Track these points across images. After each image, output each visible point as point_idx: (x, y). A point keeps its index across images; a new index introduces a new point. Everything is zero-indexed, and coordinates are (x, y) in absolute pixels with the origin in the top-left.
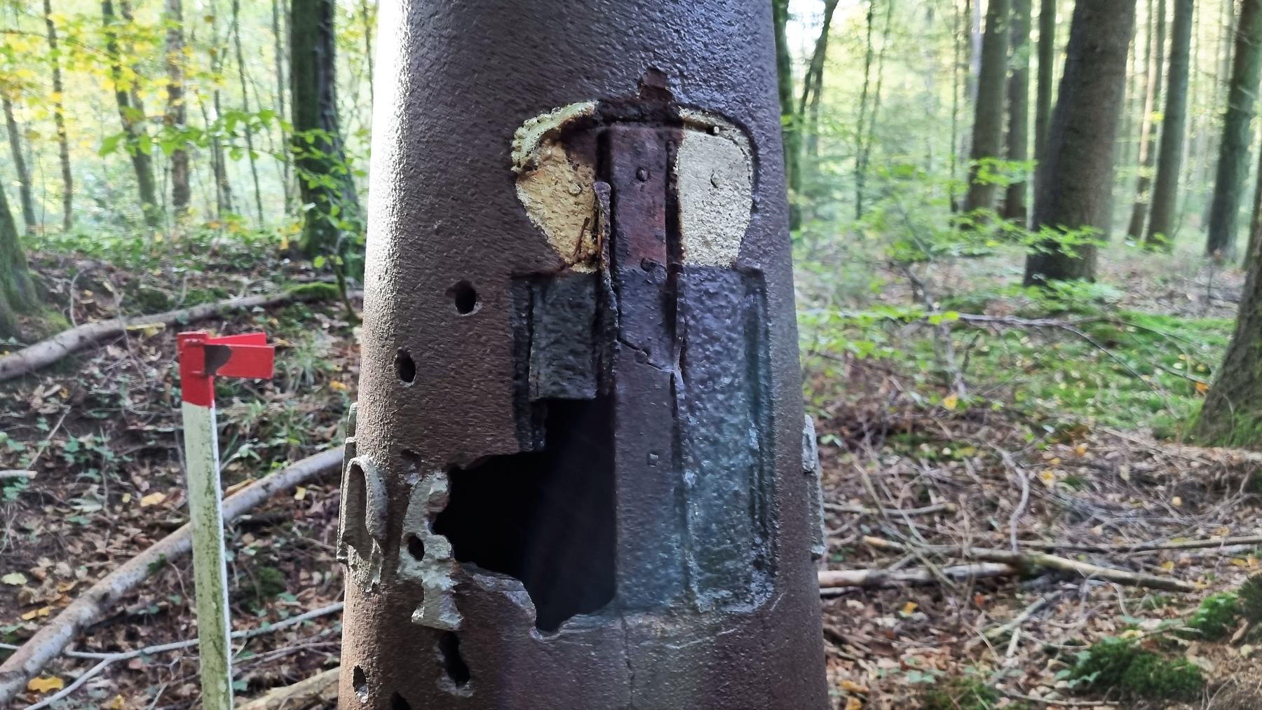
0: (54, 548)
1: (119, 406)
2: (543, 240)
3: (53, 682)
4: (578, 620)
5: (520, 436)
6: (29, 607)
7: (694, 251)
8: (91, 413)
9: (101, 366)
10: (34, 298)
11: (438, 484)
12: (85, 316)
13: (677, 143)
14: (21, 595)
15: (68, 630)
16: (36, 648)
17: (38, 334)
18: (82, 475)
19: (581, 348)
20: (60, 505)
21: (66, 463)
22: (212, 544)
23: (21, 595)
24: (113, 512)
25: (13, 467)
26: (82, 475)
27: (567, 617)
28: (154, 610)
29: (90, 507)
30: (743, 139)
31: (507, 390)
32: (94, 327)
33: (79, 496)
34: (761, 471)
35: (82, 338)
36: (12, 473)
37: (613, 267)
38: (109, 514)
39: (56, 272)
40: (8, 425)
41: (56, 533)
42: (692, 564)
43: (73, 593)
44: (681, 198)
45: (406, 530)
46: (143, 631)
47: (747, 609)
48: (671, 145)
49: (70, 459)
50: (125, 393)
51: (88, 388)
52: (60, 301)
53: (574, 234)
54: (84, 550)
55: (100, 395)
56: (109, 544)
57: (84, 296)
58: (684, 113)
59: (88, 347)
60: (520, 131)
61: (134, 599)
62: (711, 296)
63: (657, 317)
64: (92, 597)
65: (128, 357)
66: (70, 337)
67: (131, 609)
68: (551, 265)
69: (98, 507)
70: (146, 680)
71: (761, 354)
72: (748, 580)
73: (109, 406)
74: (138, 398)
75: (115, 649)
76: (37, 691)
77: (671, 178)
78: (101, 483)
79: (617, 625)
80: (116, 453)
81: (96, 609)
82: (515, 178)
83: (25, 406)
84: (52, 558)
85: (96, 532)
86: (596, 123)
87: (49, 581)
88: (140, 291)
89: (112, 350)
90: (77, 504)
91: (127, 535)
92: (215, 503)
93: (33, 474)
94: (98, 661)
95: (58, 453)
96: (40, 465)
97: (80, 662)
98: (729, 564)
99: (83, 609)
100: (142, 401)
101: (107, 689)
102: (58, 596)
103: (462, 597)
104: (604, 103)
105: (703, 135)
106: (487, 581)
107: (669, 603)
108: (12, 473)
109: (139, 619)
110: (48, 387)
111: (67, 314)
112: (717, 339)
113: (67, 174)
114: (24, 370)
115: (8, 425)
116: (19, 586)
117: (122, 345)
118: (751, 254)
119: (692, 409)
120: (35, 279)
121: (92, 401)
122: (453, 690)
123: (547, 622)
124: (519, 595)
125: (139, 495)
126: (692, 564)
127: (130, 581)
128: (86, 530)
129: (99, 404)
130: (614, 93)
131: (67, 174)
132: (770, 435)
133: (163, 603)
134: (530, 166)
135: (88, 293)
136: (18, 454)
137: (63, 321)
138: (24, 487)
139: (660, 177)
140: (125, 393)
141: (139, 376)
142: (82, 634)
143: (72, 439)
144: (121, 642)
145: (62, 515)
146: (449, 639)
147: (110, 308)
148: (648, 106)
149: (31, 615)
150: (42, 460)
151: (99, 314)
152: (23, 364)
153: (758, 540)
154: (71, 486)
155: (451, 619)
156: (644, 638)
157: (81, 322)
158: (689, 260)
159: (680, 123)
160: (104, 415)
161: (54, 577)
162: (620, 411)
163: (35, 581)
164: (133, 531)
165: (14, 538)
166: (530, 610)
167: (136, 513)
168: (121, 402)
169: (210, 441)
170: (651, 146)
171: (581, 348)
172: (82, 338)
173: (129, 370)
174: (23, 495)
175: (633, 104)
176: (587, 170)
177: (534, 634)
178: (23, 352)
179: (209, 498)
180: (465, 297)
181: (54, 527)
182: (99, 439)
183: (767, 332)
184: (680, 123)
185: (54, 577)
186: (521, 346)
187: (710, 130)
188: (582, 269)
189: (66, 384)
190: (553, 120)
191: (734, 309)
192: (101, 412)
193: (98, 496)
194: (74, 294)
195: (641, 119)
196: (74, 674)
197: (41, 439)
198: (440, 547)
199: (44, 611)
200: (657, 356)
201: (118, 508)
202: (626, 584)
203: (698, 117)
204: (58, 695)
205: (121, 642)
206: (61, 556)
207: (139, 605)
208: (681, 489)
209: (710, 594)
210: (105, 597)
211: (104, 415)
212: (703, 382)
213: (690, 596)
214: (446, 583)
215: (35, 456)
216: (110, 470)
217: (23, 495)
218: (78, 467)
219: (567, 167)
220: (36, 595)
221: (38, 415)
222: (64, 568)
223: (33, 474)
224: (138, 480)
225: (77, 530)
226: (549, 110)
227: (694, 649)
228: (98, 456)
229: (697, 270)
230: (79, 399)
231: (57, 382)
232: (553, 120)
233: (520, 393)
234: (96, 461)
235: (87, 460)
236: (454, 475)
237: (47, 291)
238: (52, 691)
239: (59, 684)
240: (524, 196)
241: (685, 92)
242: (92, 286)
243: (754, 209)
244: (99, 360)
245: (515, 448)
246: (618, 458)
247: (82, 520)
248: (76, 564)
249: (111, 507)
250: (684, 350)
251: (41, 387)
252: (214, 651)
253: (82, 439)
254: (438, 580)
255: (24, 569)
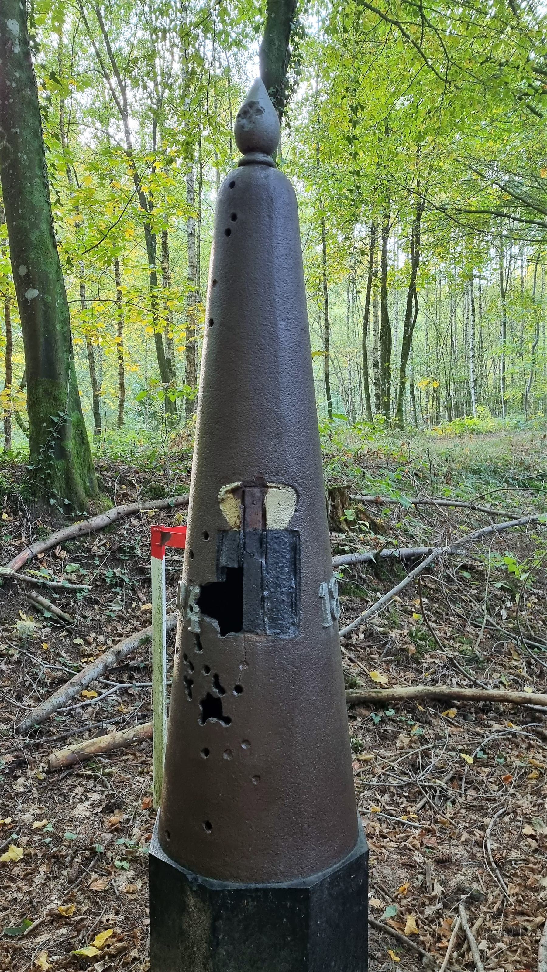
0: (98, 628)
1: (134, 553)
2: (226, 520)
3: (93, 693)
4: (232, 633)
5: (218, 577)
6: (84, 656)
7: (271, 524)
8: (120, 556)
9: (127, 529)
10: (97, 490)
11: (197, 590)
12: (121, 500)
13: (266, 493)
14: (81, 650)
15: (101, 667)
16: (86, 674)
17: (98, 510)
18: (113, 590)
19: (233, 552)
20: (102, 605)
21: (106, 583)
22: (160, 622)
23: (81, 650)
24: (127, 612)
25: (81, 583)
26: (113, 590)
27: (229, 632)
28: (142, 665)
29: (116, 608)
30: (292, 490)
31: (214, 563)
32: (126, 507)
33: (111, 601)
34: (296, 595)
35: (119, 513)
36: (81, 586)
37: (244, 529)
38: (125, 613)
39: (109, 474)
40: (80, 560)
41: (99, 620)
42: (266, 620)
43: (104, 651)
44: (267, 509)
45: (189, 603)
46: (136, 676)
47: (287, 637)
48: (264, 493)
49: (108, 581)
50: (138, 546)
51: (120, 542)
52: (108, 490)
53: (234, 519)
54: (112, 630)
55: (125, 546)
56: (123, 629)
57: (121, 488)
58: (269, 484)
59: (120, 519)
60: (221, 489)
61: (133, 659)
62: (276, 538)
63: (257, 544)
64: (113, 651)
65: (141, 525)
66: (113, 513)
67: (131, 663)
68: (228, 528)
69: (120, 608)
70: (135, 699)
71: (298, 557)
72: (288, 628)
73: (129, 553)
74: (144, 549)
75: (122, 682)
76: (86, 697)
77: (263, 504)
78: (122, 595)
79: (242, 636)
80: (131, 579)
81: (114, 658)
82: (219, 502)
83: (89, 550)
84: (96, 633)
85: (118, 622)
86: (241, 488)
87: (94, 645)
88: (152, 487)
89: (134, 521)
90: (110, 606)
91: (133, 625)
92: (162, 603)
93: (90, 587)
94: (113, 686)
95: (103, 577)
96: (94, 583)
97: (106, 686)
98: (280, 622)
99: (109, 658)
100: (146, 551)
101: (117, 701)
102: (98, 652)
103: (201, 624)
104: (244, 482)
105: (275, 490)
106: (207, 619)
107: (259, 631)
108: (81, 586)
109: (134, 669)
110: (100, 540)
111: (113, 499)
112: (278, 552)
113: (122, 384)
114: (90, 530)
115: (80, 560)
116: (80, 645)
117: (139, 518)
118: (293, 525)
119: (268, 572)
120: (98, 479)
121: (121, 550)
122: (198, 652)
123: (223, 633)
124: (215, 624)
125: (141, 604)
126: (266, 620)
127: (131, 646)
128: (113, 620)
129: (125, 552)
130: (247, 479)
131: (122, 384)
132: (300, 583)
133: (147, 663)
134: (223, 500)
135: (124, 486)
136: (84, 576)
137: (110, 503)
138: (85, 594)
139: (260, 504)
140: (138, 546)
141: (146, 537)
142: (107, 672)
143: (110, 570)
144: (125, 679)
145: (103, 611)
146: (198, 636)
147: (135, 496)
148: (258, 482)
149: (85, 660)
150: (95, 580)
151: (128, 499)
152: (89, 527)
153: (293, 616)
154: (108, 595)
155: (197, 630)
156: (250, 641)
157: (119, 504)
158: (269, 527)
159: (268, 487)
160: (127, 558)
161: (97, 643)
162: (245, 572)
163: (88, 644)
164: (136, 623)
165: (80, 620)
166: (218, 629)
167: (138, 613)
168: (135, 551)
169: (162, 575)
170: (258, 495)
171: (233, 552)
172: (119, 513)
173: (141, 532)
174: (85, 598)
175: (253, 482)
176: (239, 501)
177: (219, 636)
178: (90, 520)
179: (160, 601)
180: (206, 536)
181: (98, 617)
182: (123, 572)
183: (300, 550)
184: (268, 487)
185: (97, 643)
186: (219, 551)
187: (278, 488)
188: (236, 529)
189: (109, 539)
190: (229, 487)
191: (286, 543)
192: (125, 556)
193: (121, 602)
194: (117, 487)
195: (256, 486)
196: (103, 691)
197: (95, 569)
198: (196, 608)
199: (91, 659)
200: (257, 556)
201: (130, 610)
202: (245, 623)
203: (274, 485)
204: (94, 699)
205: (125, 679)
206: (101, 632)
207: (135, 662)
208: (263, 597)
209: (273, 630)
210: (119, 653)
211: (127, 558)
212: (273, 565)
213: (265, 630)
214: (197, 619)
215: (91, 577)
216: (127, 588)
217: (85, 598)
218: (112, 586)
219: (233, 500)
220: (88, 651)
221: (95, 555)
222: (101, 638)
223: (90, 587)
224: (141, 595)
225: (109, 620)
226: (229, 484)
227: (266, 647)
228: (122, 580)
229: (272, 530)
230: (115, 548)
231: (105, 538)
232: (229, 487)
233: (218, 565)
234: (121, 583)
235: (116, 582)
236: (202, 588)
237: (103, 485)
238: (93, 697)
239: (96, 695)
240: (221, 508)
241: (270, 478)
242: (126, 482)
243: (296, 511)
244: (126, 527)
245: (216, 580)
246: (244, 586)
247: (112, 614)
248: (107, 638)
249: (126, 609)
250: (266, 555)
251: (97, 540)
252: (158, 672)
253: (115, 571)
254: (195, 619)
255: (83, 637)
